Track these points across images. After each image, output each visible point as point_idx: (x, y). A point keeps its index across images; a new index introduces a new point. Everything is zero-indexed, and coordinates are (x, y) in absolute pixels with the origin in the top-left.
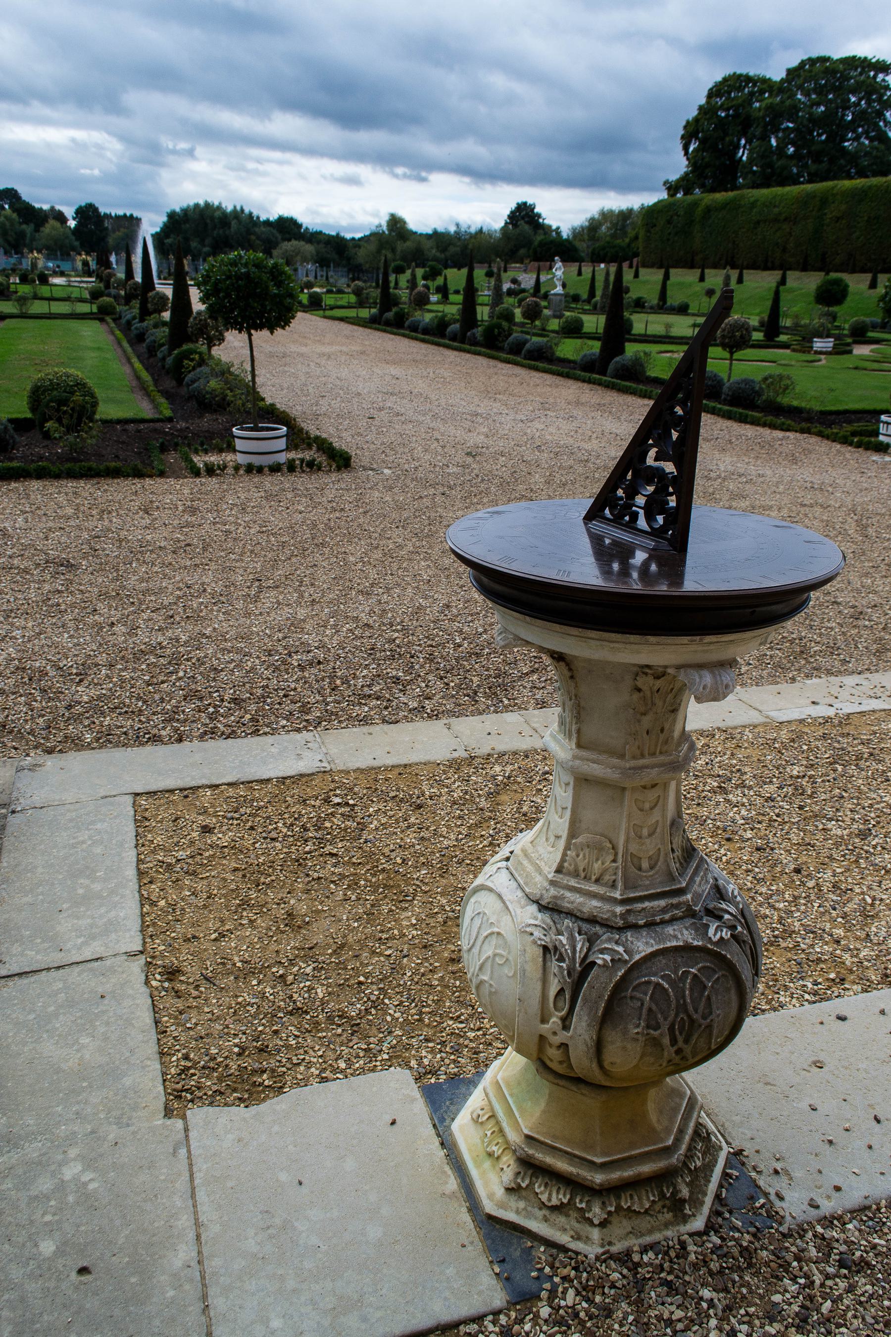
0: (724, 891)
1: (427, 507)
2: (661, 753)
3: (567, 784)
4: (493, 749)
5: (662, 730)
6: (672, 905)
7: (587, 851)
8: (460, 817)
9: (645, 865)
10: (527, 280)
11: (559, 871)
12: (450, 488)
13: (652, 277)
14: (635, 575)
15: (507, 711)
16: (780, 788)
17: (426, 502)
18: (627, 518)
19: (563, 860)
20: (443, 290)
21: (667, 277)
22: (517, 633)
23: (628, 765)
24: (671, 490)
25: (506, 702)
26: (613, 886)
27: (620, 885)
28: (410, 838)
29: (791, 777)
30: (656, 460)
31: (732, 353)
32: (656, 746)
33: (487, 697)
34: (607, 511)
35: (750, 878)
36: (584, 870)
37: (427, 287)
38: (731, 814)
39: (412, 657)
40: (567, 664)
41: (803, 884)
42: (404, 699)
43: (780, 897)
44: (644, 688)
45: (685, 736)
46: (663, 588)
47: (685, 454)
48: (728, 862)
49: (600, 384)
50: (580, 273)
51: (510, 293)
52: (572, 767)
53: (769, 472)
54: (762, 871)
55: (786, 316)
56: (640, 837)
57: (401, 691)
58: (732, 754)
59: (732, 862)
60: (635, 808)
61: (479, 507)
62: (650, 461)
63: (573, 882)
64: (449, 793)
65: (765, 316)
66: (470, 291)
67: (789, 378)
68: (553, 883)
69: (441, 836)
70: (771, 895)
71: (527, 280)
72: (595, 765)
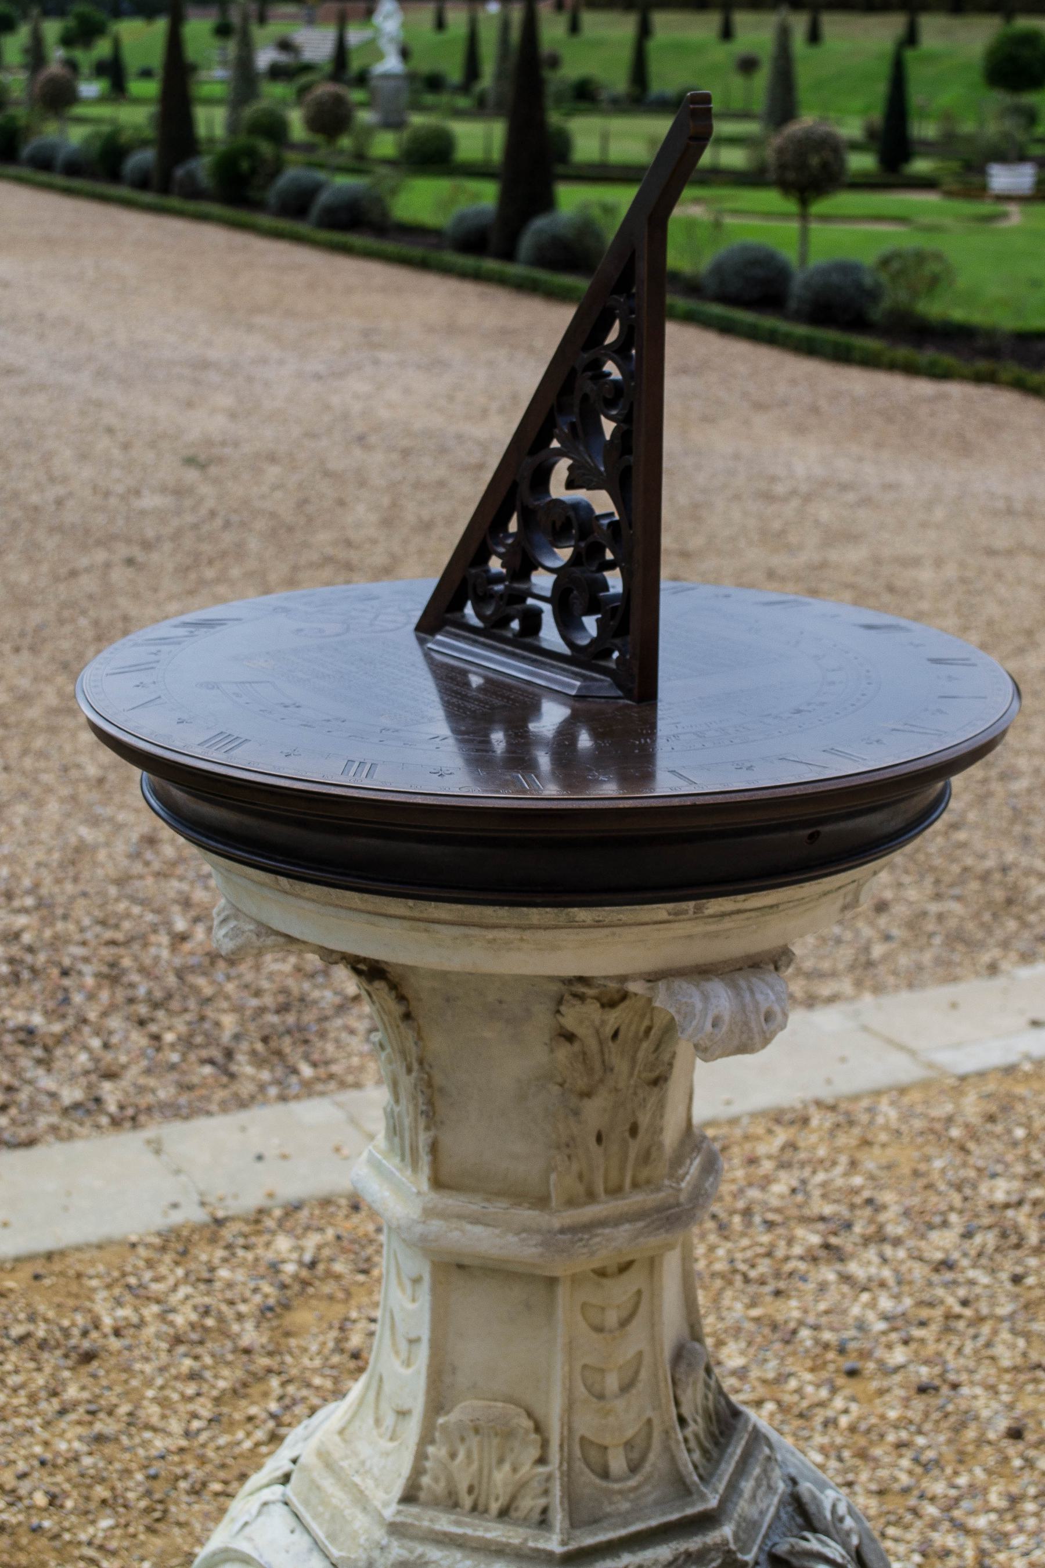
0: (812, 1509)
1: (90, 597)
2: (635, 1185)
3: (417, 1281)
4: (271, 1196)
5: (634, 1131)
6: (688, 1555)
7: (474, 1441)
8: (193, 1376)
9: (617, 1463)
10: (316, 43)
11: (409, 1498)
12: (147, 546)
13: (611, 31)
14: (544, 760)
15: (310, 1095)
16: (968, 1235)
17: (88, 583)
18: (515, 625)
19: (418, 1471)
20: (113, 71)
21: (645, 31)
22: (264, 918)
23: (556, 1223)
24: (609, 556)
25: (307, 1071)
26: (543, 1522)
27: (558, 1518)
28: (69, 1440)
29: (991, 1207)
30: (570, 485)
31: (804, 203)
32: (622, 1169)
33: (258, 1060)
34: (469, 610)
35: (905, 1463)
36: (471, 1490)
37: (72, 65)
38: (856, 1310)
39: (65, 973)
40: (394, 986)
41: (1030, 1463)
42: (47, 1082)
43: (978, 1503)
44: (580, 1031)
45: (691, 1138)
46: (608, 790)
47: (635, 469)
48: (853, 1429)
49: (501, 281)
50: (440, 24)
51: (277, 72)
52: (423, 1238)
53: (907, 478)
54: (932, 1443)
55: (924, 115)
56: (601, 1397)
57: (39, 1062)
58: (853, 1164)
59: (863, 1426)
60: (583, 1326)
61: (221, 590)
62: (558, 489)
63: (445, 1523)
64: (162, 1317)
65: (877, 116)
66: (177, 73)
67: (938, 257)
68: (396, 1529)
69: (148, 1427)
70: (957, 1500)
71: (316, 43)
72: (478, 1229)
